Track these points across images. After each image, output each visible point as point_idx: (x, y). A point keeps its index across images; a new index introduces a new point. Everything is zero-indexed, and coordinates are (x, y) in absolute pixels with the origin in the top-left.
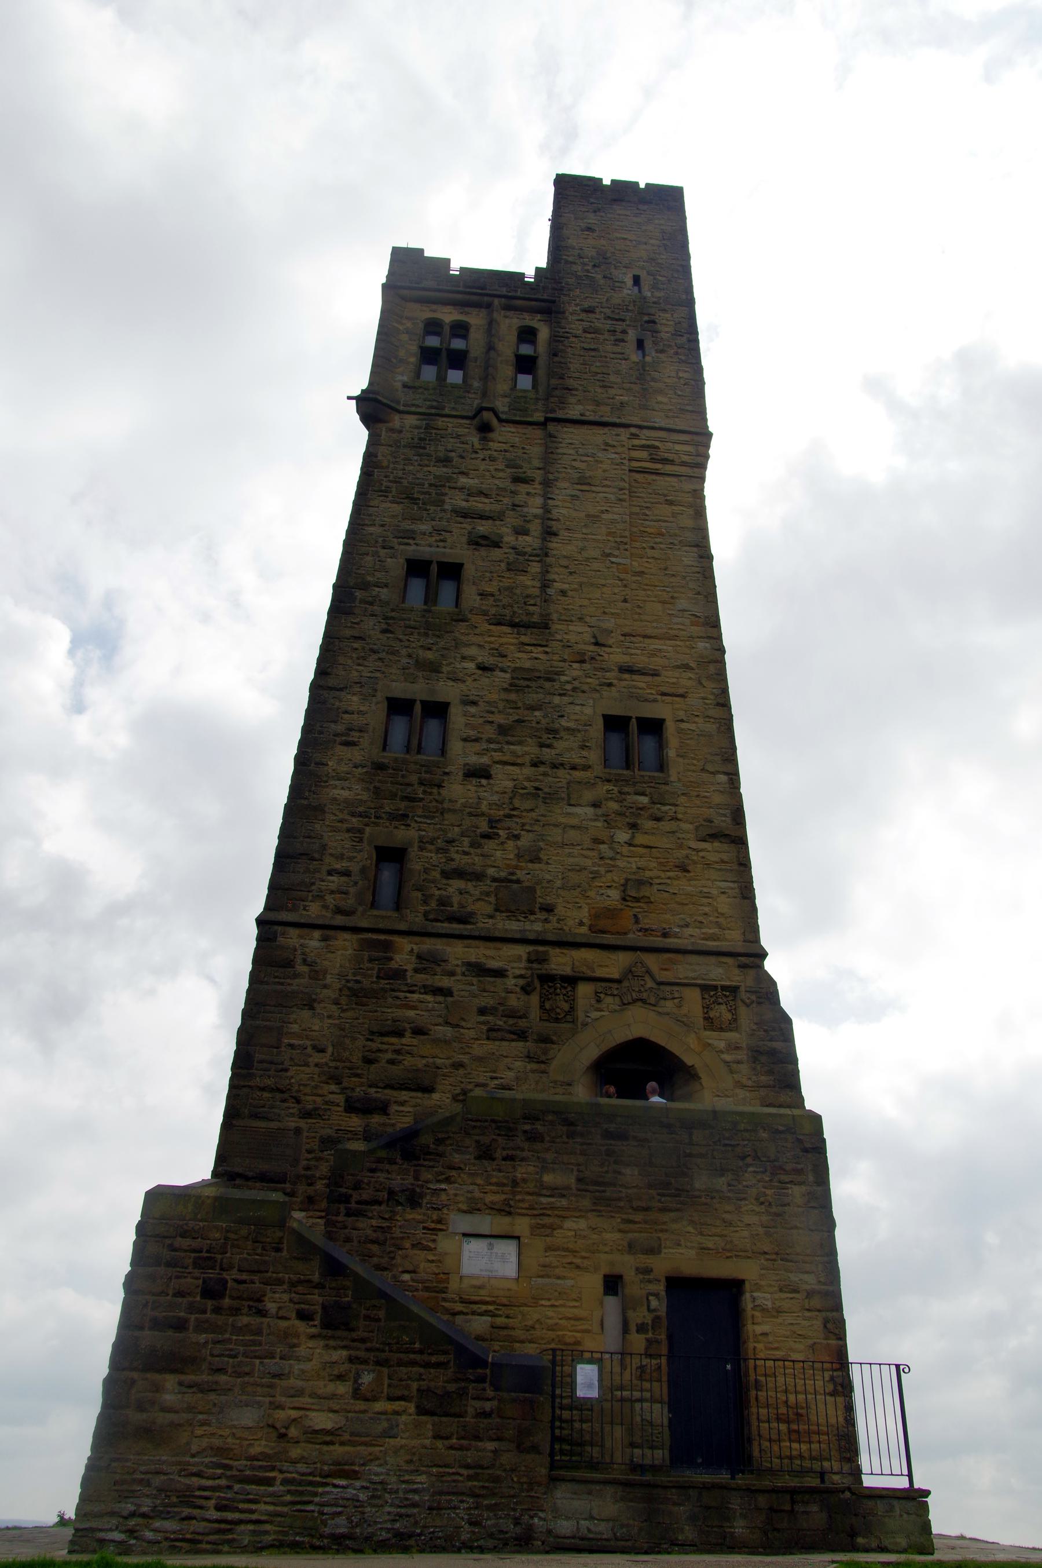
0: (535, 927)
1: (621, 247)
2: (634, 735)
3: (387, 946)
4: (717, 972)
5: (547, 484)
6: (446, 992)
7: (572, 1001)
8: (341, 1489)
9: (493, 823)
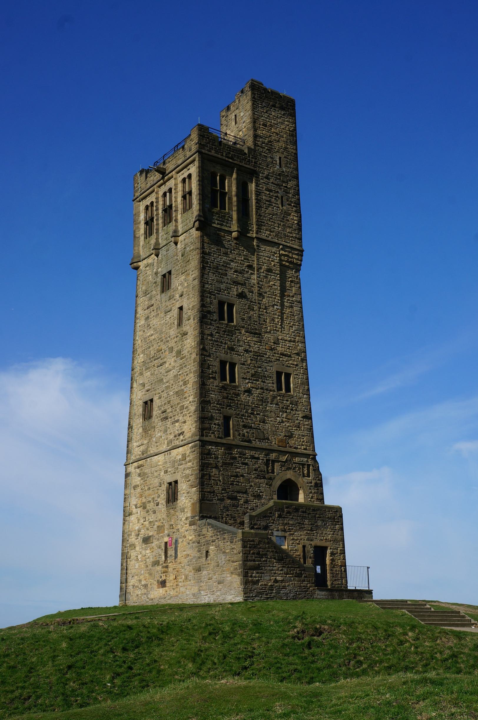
0: (264, 445)
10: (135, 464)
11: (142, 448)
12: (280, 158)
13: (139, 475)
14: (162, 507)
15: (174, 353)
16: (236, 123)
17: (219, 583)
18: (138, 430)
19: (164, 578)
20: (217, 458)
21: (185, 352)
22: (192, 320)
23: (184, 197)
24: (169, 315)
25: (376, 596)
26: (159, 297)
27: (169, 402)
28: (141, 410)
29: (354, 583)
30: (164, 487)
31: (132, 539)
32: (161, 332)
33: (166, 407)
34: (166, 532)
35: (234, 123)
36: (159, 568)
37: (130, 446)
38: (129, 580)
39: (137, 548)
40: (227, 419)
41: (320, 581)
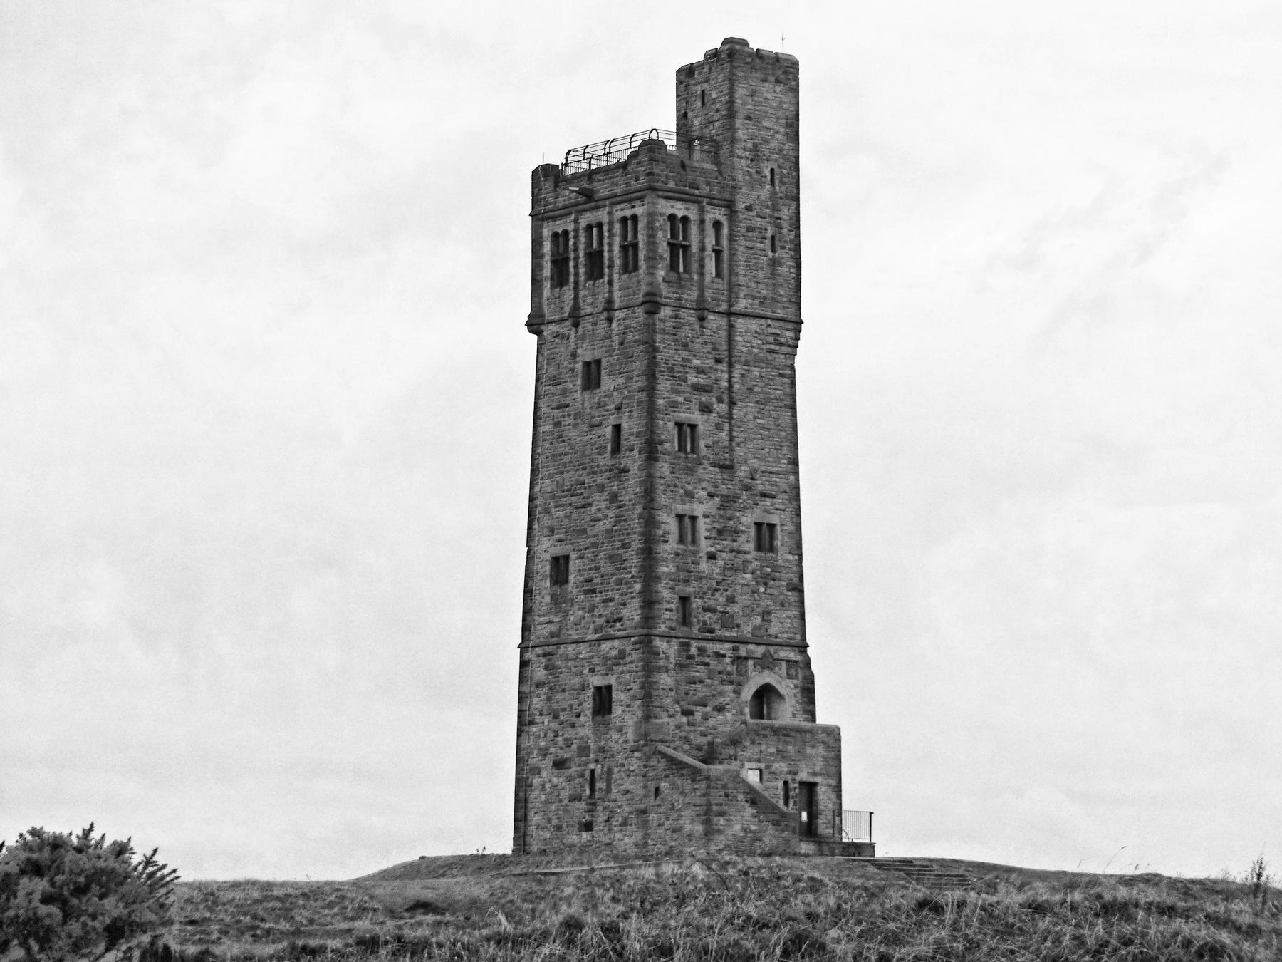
0: (734, 634)
1: (740, 95)
2: (765, 535)
3: (688, 645)
4: (792, 655)
5: (731, 366)
6: (707, 664)
7: (746, 667)
8: (758, 843)
9: (718, 583)
10: (539, 651)
11: (552, 628)
12: (772, 170)
13: (546, 668)
14: (586, 718)
15: (605, 495)
16: (703, 104)
17: (674, 831)
18: (543, 600)
19: (588, 818)
20: (667, 658)
21: (625, 498)
22: (636, 452)
23: (624, 248)
24: (599, 431)
25: (880, 853)
26: (578, 395)
27: (598, 568)
28: (548, 568)
29: (852, 833)
30: (590, 692)
31: (534, 760)
32: (583, 455)
33: (593, 574)
34: (592, 756)
35: (699, 104)
36: (582, 805)
37: (529, 618)
38: (529, 818)
39: (544, 774)
40: (684, 600)
41: (809, 831)
